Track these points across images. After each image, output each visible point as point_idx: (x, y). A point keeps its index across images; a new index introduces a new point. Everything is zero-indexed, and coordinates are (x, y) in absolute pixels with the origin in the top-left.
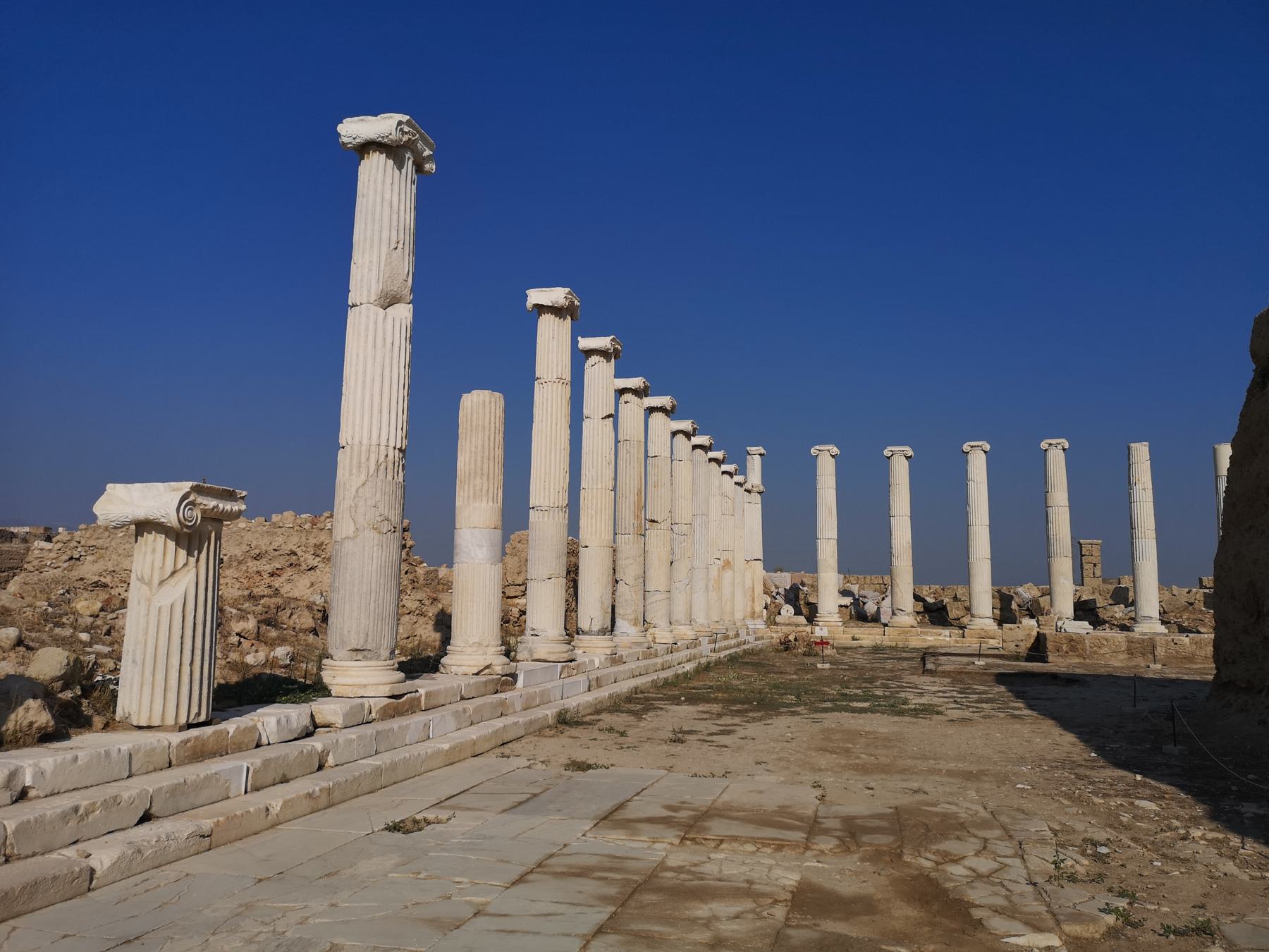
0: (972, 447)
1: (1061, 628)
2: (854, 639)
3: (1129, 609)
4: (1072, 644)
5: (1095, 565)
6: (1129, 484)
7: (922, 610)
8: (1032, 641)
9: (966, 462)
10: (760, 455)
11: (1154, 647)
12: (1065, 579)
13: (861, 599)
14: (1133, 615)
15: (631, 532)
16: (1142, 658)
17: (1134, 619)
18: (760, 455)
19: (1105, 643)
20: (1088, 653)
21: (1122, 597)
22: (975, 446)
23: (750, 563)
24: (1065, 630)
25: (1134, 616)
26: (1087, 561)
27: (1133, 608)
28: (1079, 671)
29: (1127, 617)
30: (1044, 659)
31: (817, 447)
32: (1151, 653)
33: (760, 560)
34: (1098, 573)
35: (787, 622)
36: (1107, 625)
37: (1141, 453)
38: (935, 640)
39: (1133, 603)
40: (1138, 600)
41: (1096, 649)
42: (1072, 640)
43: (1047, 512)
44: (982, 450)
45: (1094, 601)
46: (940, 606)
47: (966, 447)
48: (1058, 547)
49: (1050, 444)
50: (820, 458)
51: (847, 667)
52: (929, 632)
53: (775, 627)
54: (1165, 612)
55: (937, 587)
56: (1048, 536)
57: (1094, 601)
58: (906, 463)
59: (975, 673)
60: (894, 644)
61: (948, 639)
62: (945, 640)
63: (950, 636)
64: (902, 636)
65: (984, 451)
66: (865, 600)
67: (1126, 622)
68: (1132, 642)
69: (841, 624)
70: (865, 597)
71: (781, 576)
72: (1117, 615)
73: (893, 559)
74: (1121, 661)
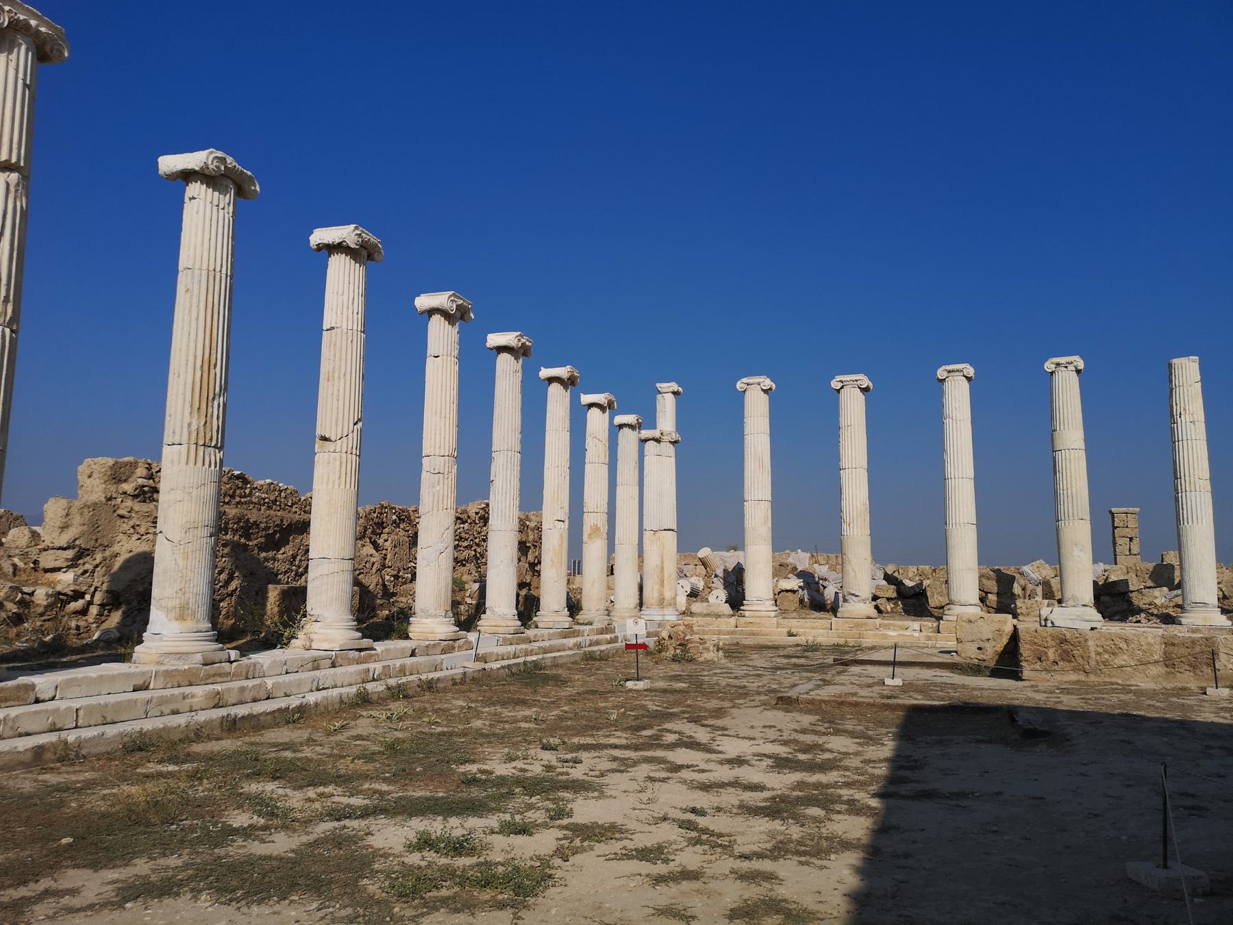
0: (949, 372)
1: (1046, 620)
2: (791, 634)
3: (1175, 592)
4: (1065, 647)
5: (1131, 539)
6: (1171, 440)
7: (894, 595)
8: (1005, 640)
9: (941, 393)
10: (674, 393)
11: (1214, 654)
12: (1081, 550)
13: (821, 582)
14: (1179, 600)
15: (184, 440)
16: (1192, 674)
17: (1180, 606)
18: (674, 393)
19: (1123, 645)
20: (1093, 663)
21: (1165, 576)
22: (953, 371)
23: (657, 534)
24: (1052, 623)
25: (1180, 603)
26: (1121, 534)
27: (1179, 592)
28: (1070, 702)
29: (1172, 604)
30: (1017, 676)
31: (745, 380)
32: (1208, 665)
33: (673, 530)
34: (1135, 549)
35: (705, 612)
36: (1143, 615)
37: (1188, 371)
38: (900, 635)
39: (1180, 586)
40: (1186, 578)
41: (1106, 656)
42: (1064, 641)
43: (1054, 458)
44: (964, 376)
45: (1126, 582)
46: (918, 590)
47: (941, 373)
48: (1070, 505)
49: (1058, 364)
50: (748, 395)
51: (197, 748)
52: (892, 625)
53: (690, 618)
54: (1225, 597)
55: (927, 567)
56: (1056, 492)
57: (1126, 582)
58: (861, 397)
59: (868, 704)
60: (842, 641)
61: (916, 634)
62: (912, 635)
63: (921, 631)
64: (855, 631)
65: (966, 377)
66: (825, 584)
67: (1171, 611)
68: (1173, 645)
69: (773, 614)
70: (826, 580)
71: (734, 556)
72: (1157, 602)
73: (844, 526)
74: (1154, 678)
